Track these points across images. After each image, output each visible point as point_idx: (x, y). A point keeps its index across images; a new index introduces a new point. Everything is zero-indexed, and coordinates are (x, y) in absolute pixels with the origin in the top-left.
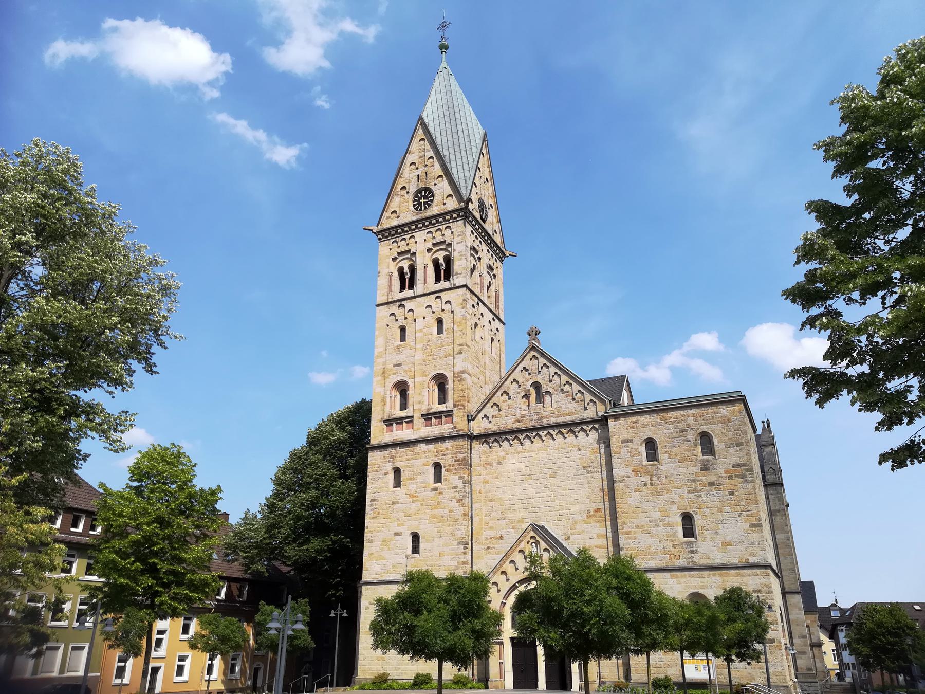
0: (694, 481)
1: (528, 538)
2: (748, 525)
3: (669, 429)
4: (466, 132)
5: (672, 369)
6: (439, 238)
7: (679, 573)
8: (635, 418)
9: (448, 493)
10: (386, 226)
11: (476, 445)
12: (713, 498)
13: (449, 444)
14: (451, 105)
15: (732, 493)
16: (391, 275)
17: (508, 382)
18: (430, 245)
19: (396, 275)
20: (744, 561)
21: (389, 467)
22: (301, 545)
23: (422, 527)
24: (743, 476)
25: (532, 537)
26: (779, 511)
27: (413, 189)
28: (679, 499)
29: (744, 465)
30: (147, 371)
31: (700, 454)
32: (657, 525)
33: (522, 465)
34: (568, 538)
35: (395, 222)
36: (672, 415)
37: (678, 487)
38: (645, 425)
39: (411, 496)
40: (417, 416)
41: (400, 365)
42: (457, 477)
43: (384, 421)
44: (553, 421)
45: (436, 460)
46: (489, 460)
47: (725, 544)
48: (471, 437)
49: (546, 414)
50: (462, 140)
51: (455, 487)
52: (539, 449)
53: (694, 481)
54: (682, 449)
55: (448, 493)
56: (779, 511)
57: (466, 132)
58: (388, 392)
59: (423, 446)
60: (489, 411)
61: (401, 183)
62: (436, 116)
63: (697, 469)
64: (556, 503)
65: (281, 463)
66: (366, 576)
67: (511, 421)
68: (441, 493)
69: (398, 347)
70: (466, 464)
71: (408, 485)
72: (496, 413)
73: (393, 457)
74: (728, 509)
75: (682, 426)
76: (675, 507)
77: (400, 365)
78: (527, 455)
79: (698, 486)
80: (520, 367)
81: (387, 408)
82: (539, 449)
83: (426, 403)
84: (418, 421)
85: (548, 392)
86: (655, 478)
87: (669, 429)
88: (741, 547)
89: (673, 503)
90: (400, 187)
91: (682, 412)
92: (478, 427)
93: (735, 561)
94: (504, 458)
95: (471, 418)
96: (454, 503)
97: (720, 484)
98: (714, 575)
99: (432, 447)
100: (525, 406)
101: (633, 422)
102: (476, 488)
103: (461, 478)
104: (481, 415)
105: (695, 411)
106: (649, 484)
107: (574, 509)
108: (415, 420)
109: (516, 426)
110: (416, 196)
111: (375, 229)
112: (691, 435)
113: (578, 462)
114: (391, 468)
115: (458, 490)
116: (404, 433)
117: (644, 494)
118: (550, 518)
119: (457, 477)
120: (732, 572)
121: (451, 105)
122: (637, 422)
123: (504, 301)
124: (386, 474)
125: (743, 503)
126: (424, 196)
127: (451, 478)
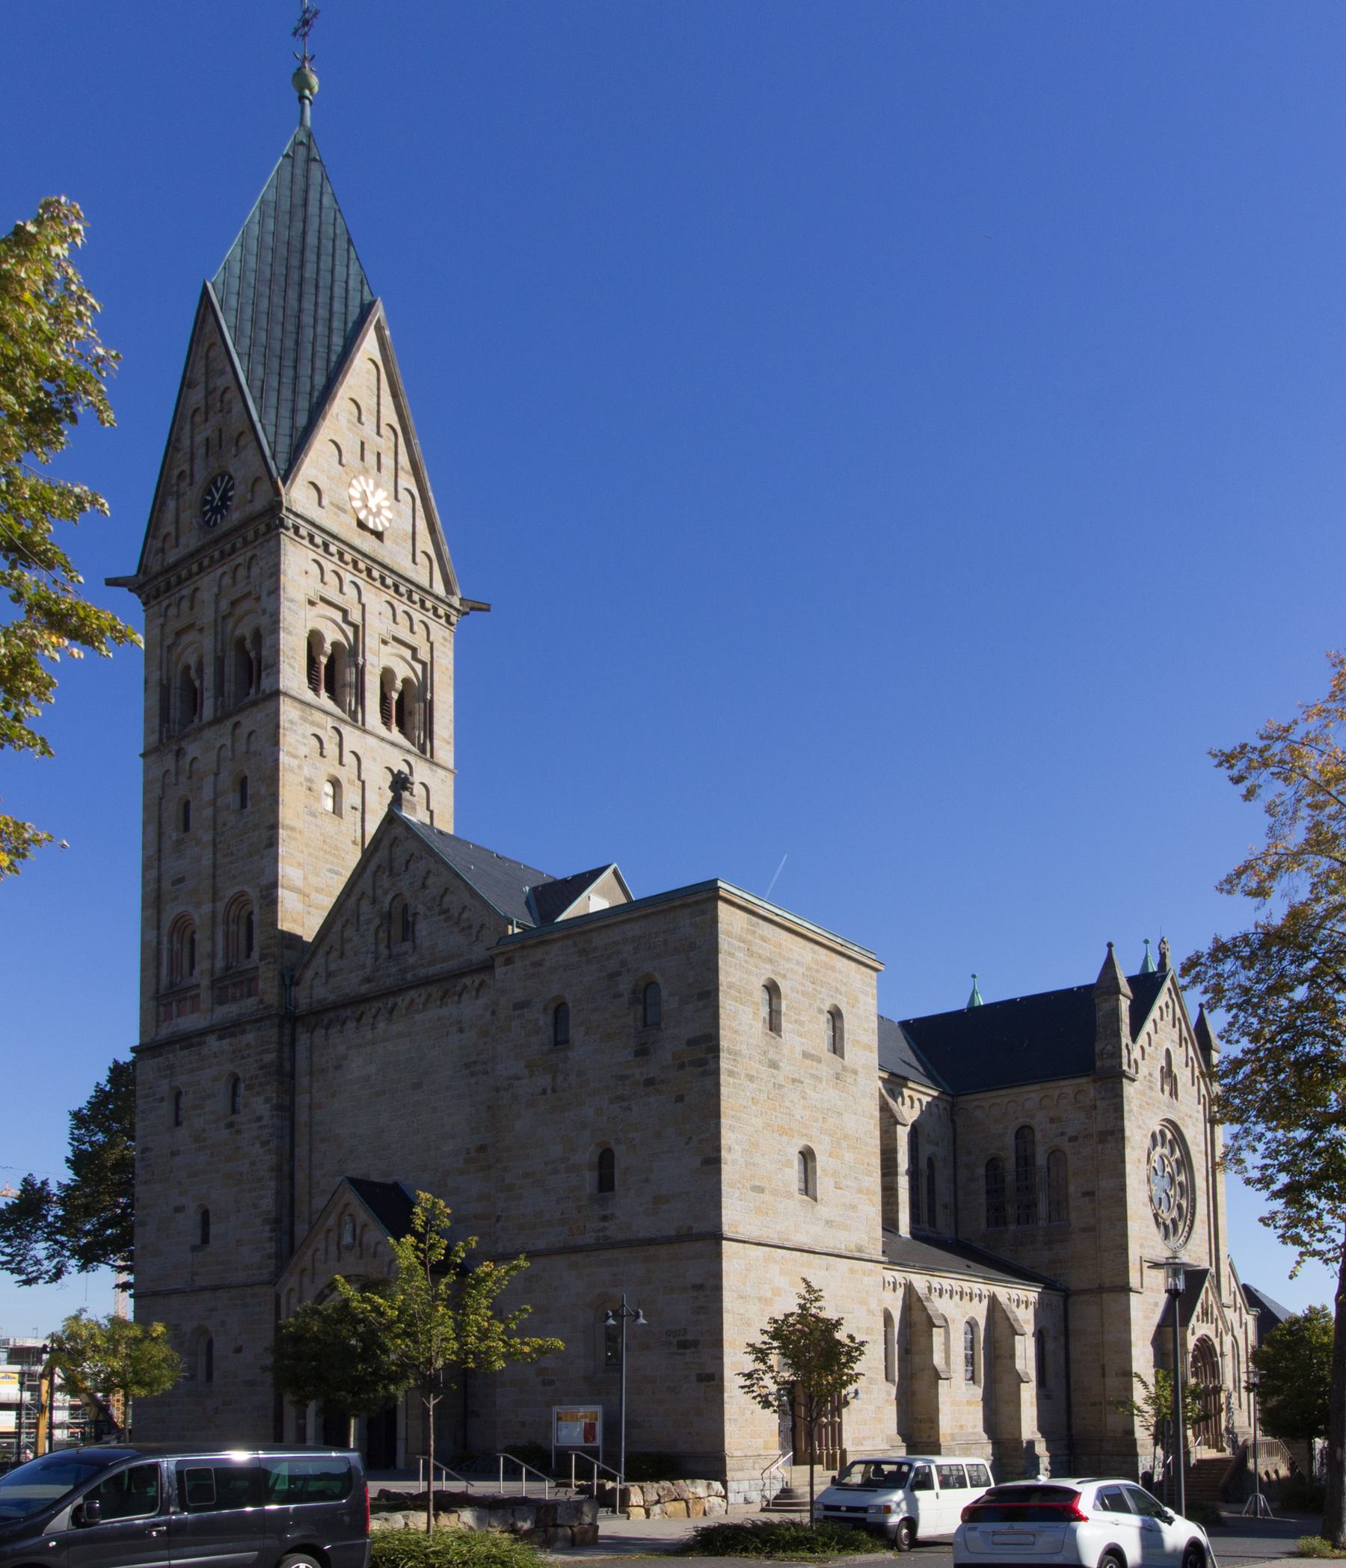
15: (680, 1098)
21: (164, 1087)
30: (28, 1282)
41: (181, 880)
42: (261, 1099)
51: (259, 1119)
53: (622, 1078)
65: (81, 1098)
68: (238, 1132)
70: (285, 1076)
77: (181, 880)
101: (534, 964)
106: (549, 1091)
115: (264, 1122)
119: (261, 1099)
122: (539, 964)
124: (162, 1099)
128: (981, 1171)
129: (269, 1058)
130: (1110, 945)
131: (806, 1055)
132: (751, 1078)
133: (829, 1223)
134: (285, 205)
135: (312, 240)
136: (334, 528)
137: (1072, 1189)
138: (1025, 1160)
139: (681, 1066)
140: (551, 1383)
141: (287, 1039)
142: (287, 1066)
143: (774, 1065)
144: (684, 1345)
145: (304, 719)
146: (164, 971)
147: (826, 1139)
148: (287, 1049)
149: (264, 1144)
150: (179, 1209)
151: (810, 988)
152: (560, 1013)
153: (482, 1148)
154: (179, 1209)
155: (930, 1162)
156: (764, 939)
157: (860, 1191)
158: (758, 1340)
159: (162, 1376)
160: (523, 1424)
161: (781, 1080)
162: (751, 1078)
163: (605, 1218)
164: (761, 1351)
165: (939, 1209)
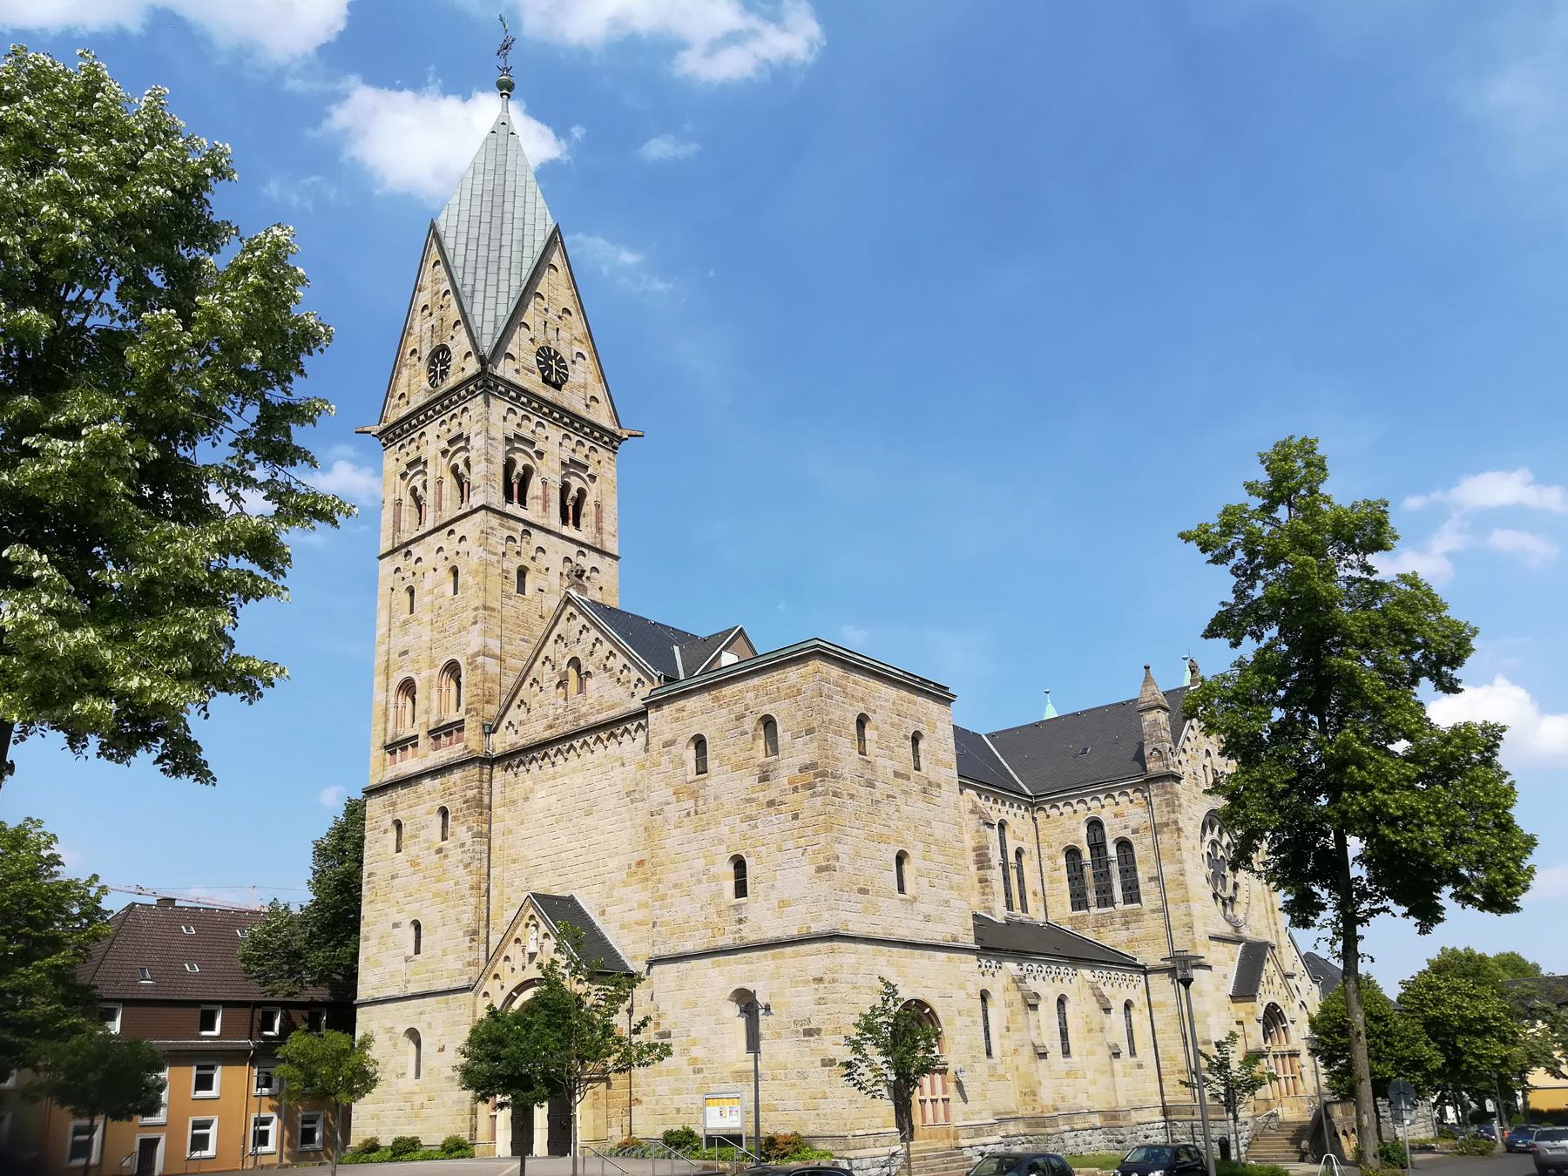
0: (749, 800)
1: (526, 920)
2: (813, 867)
3: (723, 716)
4: (517, 235)
5: (1450, 555)
6: (455, 431)
7: (721, 958)
8: (681, 703)
9: (455, 855)
10: (392, 419)
11: (498, 772)
12: (773, 826)
13: (457, 776)
14: (499, 192)
15: (796, 817)
16: (399, 503)
17: (538, 663)
18: (444, 444)
19: (408, 500)
20: (804, 931)
22: (335, 947)
23: (424, 911)
24: (811, 786)
25: (532, 917)
26: (1167, 825)
27: (426, 352)
28: (730, 835)
29: (813, 766)
31: (761, 754)
32: (699, 881)
33: (553, 799)
34: (603, 913)
35: (404, 412)
36: (727, 691)
37: (728, 815)
38: (693, 714)
39: (414, 864)
40: (422, 733)
41: (405, 653)
43: (386, 747)
44: (593, 719)
45: (441, 803)
46: (515, 797)
47: (783, 904)
48: (490, 761)
49: (584, 710)
50: (506, 252)
51: (463, 845)
52: (574, 771)
53: (749, 800)
54: (737, 749)
55: (455, 855)
56: (1167, 825)
57: (517, 235)
58: (392, 700)
59: (427, 782)
60: (514, 714)
61: (412, 343)
62: (465, 217)
63: (754, 780)
64: (591, 857)
66: (363, 993)
67: (541, 728)
68: (446, 856)
69: (406, 623)
70: (481, 807)
71: (411, 849)
72: (524, 716)
73: (393, 804)
74: (790, 844)
75: (739, 708)
76: (723, 848)
77: (405, 653)
78: (559, 781)
79: (752, 810)
80: (553, 636)
81: (391, 725)
82: (574, 771)
83: (435, 711)
84: (424, 742)
85: (588, 673)
86: (701, 802)
87: (723, 716)
88: (802, 908)
89: (721, 841)
90: (409, 351)
91: (740, 685)
92: (501, 742)
93: (793, 932)
94: (532, 791)
95: (490, 729)
96: (461, 871)
97: (782, 803)
98: (766, 957)
99: (437, 782)
100: (561, 701)
101: (678, 710)
102: (495, 843)
103: (470, 829)
104: (505, 723)
105: (756, 681)
107: (613, 863)
108: (421, 741)
109: (547, 735)
110: (432, 363)
111: (376, 429)
112: (750, 723)
113: (620, 787)
114: (390, 822)
116: (409, 764)
117: (685, 829)
118: (582, 882)
120: (788, 950)
121: (499, 192)
123: (621, 517)
124: (386, 831)
125: (809, 831)
126: (440, 358)
127: (461, 831)
128: (1062, 861)
129: (470, 794)
130: (1147, 668)
131: (897, 774)
132: (852, 796)
133: (927, 918)
134: (490, 166)
135: (509, 187)
136: (526, 385)
137: (1140, 874)
138: (1098, 847)
139: (795, 790)
140: (700, 1071)
141: (486, 777)
142: (486, 799)
143: (871, 785)
144: (809, 1033)
145: (502, 525)
146: (391, 725)
147: (920, 846)
148: (486, 785)
149: (467, 866)
150: (396, 925)
151: (896, 719)
152: (700, 743)
153: (641, 863)
154: (396, 925)
155: (1019, 853)
156: (855, 683)
157: (951, 888)
158: (854, 1033)
159: (186, 576)
160: (678, 1110)
161: (878, 796)
162: (852, 796)
163: (740, 921)
164: (855, 1042)
165: (1029, 896)
